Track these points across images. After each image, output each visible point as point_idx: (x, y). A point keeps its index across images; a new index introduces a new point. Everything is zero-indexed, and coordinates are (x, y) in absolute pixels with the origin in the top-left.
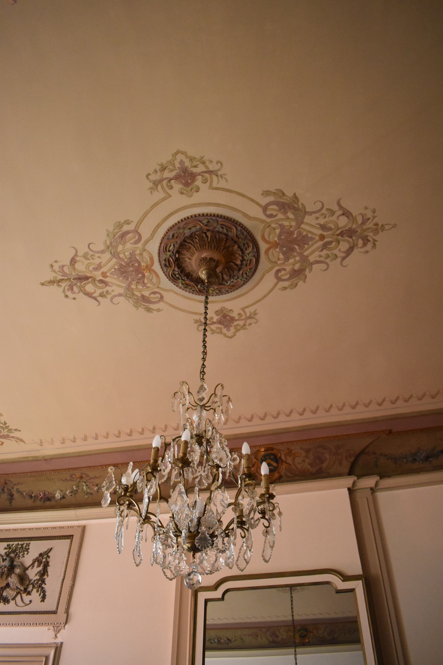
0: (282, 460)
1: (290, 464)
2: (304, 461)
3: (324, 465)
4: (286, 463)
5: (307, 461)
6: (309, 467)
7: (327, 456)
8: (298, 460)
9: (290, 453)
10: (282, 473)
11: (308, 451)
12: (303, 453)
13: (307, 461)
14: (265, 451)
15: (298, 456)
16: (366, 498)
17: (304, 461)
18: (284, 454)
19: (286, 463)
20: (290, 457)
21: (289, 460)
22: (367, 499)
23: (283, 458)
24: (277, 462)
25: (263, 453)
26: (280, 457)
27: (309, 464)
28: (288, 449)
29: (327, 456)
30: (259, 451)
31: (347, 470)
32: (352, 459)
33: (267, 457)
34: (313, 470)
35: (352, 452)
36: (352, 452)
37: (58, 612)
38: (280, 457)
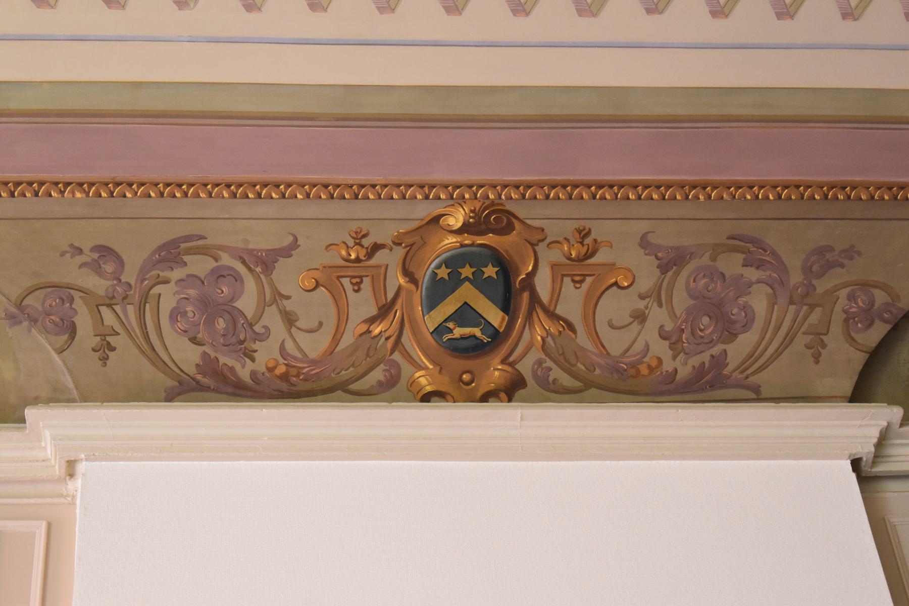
0: (535, 299)
1: (571, 327)
2: (640, 317)
3: (737, 350)
4: (552, 316)
5: (658, 316)
6: (661, 349)
7: (759, 301)
8: (614, 306)
9: (582, 262)
10: (525, 367)
11: (671, 262)
12: (647, 274)
13: (658, 316)
14: (465, 229)
15: (616, 284)
16: (44, 525)
17: (640, 317)
18: (554, 266)
19: (552, 316)
20: (578, 283)
21: (571, 302)
22: (49, 527)
23: (543, 285)
24: (507, 305)
25: (451, 240)
26: (531, 275)
27: (663, 336)
28: (583, 234)
29: (759, 301)
30: (436, 220)
31: (847, 386)
32: (879, 331)
33: (467, 271)
34: (684, 369)
35: (880, 297)
36: (880, 297)
37: (797, 15)
38: (531, 275)
